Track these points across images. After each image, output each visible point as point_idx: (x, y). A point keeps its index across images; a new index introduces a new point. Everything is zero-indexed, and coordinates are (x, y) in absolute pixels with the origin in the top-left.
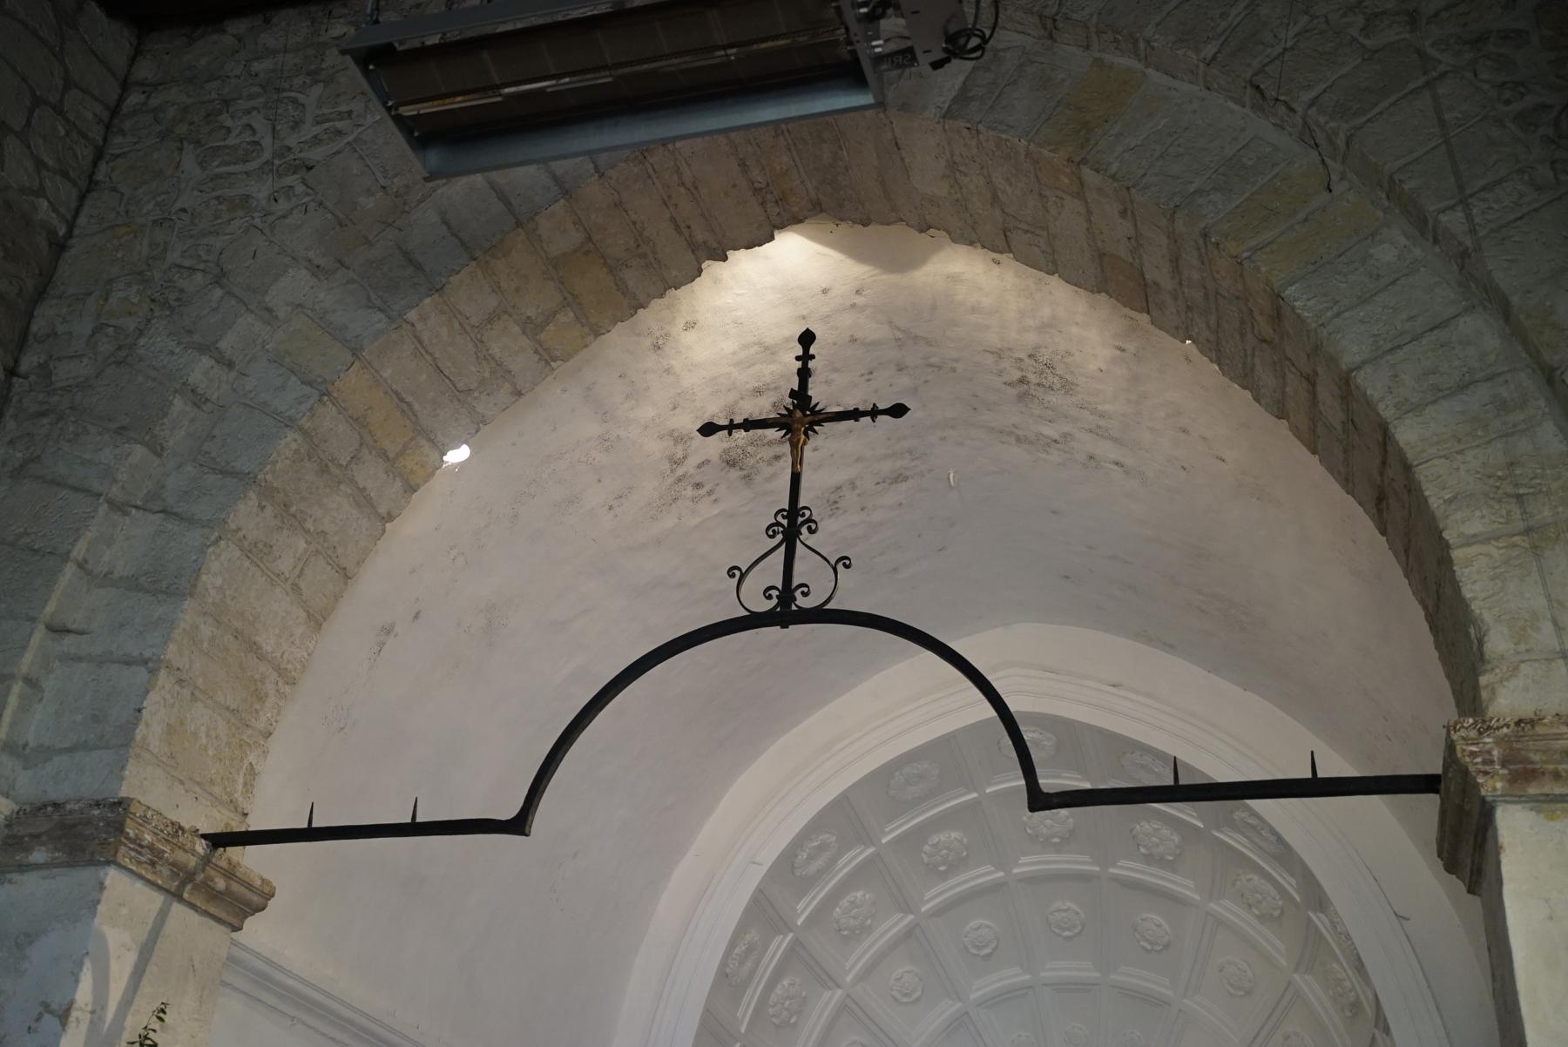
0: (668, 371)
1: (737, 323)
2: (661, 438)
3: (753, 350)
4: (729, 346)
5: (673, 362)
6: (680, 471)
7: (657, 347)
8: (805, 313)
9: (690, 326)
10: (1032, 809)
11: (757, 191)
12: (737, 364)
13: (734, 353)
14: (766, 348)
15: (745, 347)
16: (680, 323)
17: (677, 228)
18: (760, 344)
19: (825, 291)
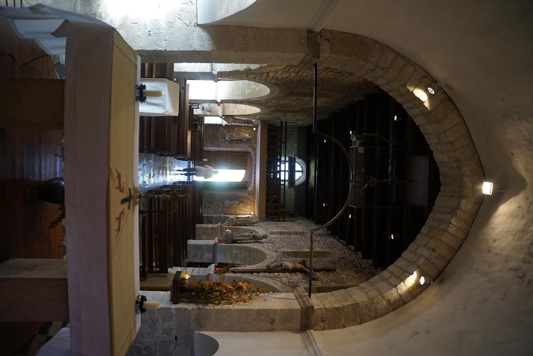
0: (496, 254)
1: (507, 232)
2: (508, 272)
3: (518, 234)
4: (510, 238)
5: (496, 251)
6: (527, 280)
7: (489, 251)
8: (521, 216)
9: (494, 241)
10: (63, 81)
11: (451, 196)
12: (518, 240)
13: (513, 239)
14: (522, 231)
15: (515, 235)
16: (491, 243)
17: (443, 213)
18: (518, 232)
19: (519, 207)
